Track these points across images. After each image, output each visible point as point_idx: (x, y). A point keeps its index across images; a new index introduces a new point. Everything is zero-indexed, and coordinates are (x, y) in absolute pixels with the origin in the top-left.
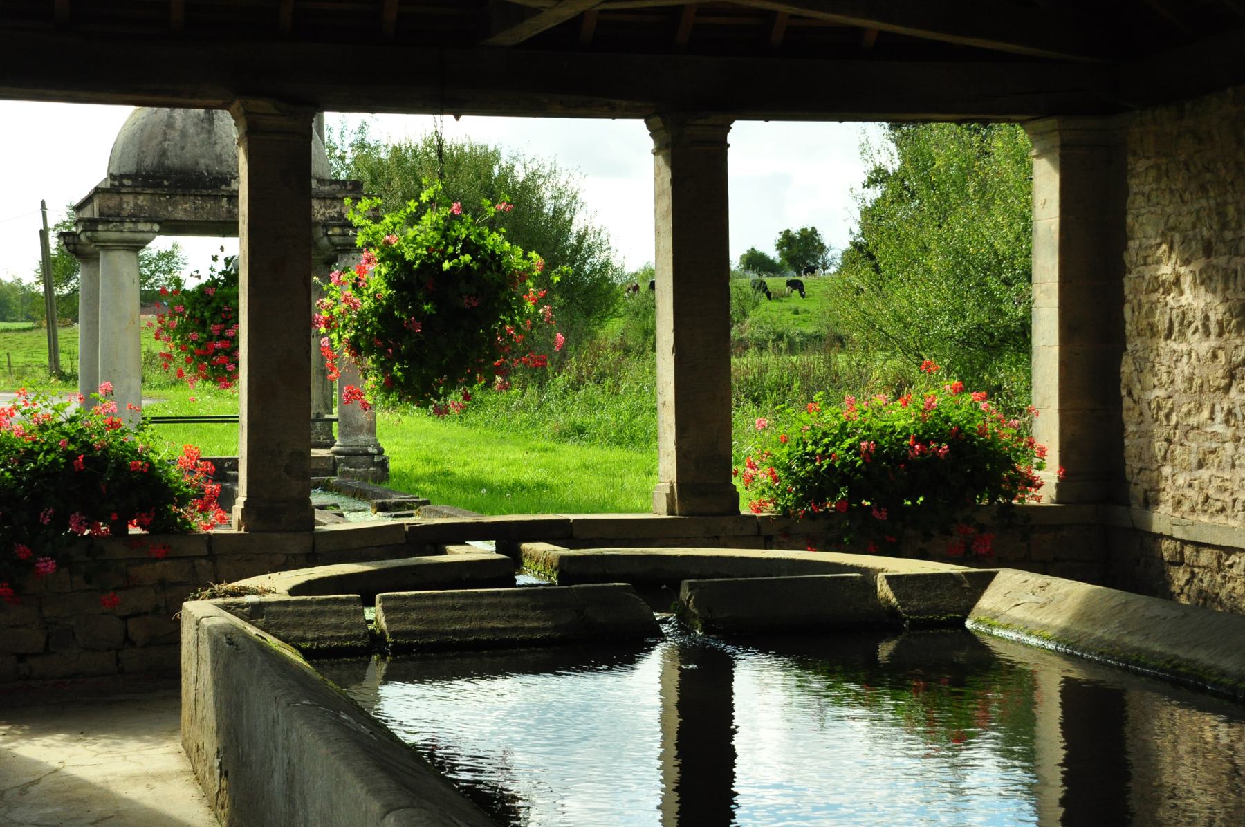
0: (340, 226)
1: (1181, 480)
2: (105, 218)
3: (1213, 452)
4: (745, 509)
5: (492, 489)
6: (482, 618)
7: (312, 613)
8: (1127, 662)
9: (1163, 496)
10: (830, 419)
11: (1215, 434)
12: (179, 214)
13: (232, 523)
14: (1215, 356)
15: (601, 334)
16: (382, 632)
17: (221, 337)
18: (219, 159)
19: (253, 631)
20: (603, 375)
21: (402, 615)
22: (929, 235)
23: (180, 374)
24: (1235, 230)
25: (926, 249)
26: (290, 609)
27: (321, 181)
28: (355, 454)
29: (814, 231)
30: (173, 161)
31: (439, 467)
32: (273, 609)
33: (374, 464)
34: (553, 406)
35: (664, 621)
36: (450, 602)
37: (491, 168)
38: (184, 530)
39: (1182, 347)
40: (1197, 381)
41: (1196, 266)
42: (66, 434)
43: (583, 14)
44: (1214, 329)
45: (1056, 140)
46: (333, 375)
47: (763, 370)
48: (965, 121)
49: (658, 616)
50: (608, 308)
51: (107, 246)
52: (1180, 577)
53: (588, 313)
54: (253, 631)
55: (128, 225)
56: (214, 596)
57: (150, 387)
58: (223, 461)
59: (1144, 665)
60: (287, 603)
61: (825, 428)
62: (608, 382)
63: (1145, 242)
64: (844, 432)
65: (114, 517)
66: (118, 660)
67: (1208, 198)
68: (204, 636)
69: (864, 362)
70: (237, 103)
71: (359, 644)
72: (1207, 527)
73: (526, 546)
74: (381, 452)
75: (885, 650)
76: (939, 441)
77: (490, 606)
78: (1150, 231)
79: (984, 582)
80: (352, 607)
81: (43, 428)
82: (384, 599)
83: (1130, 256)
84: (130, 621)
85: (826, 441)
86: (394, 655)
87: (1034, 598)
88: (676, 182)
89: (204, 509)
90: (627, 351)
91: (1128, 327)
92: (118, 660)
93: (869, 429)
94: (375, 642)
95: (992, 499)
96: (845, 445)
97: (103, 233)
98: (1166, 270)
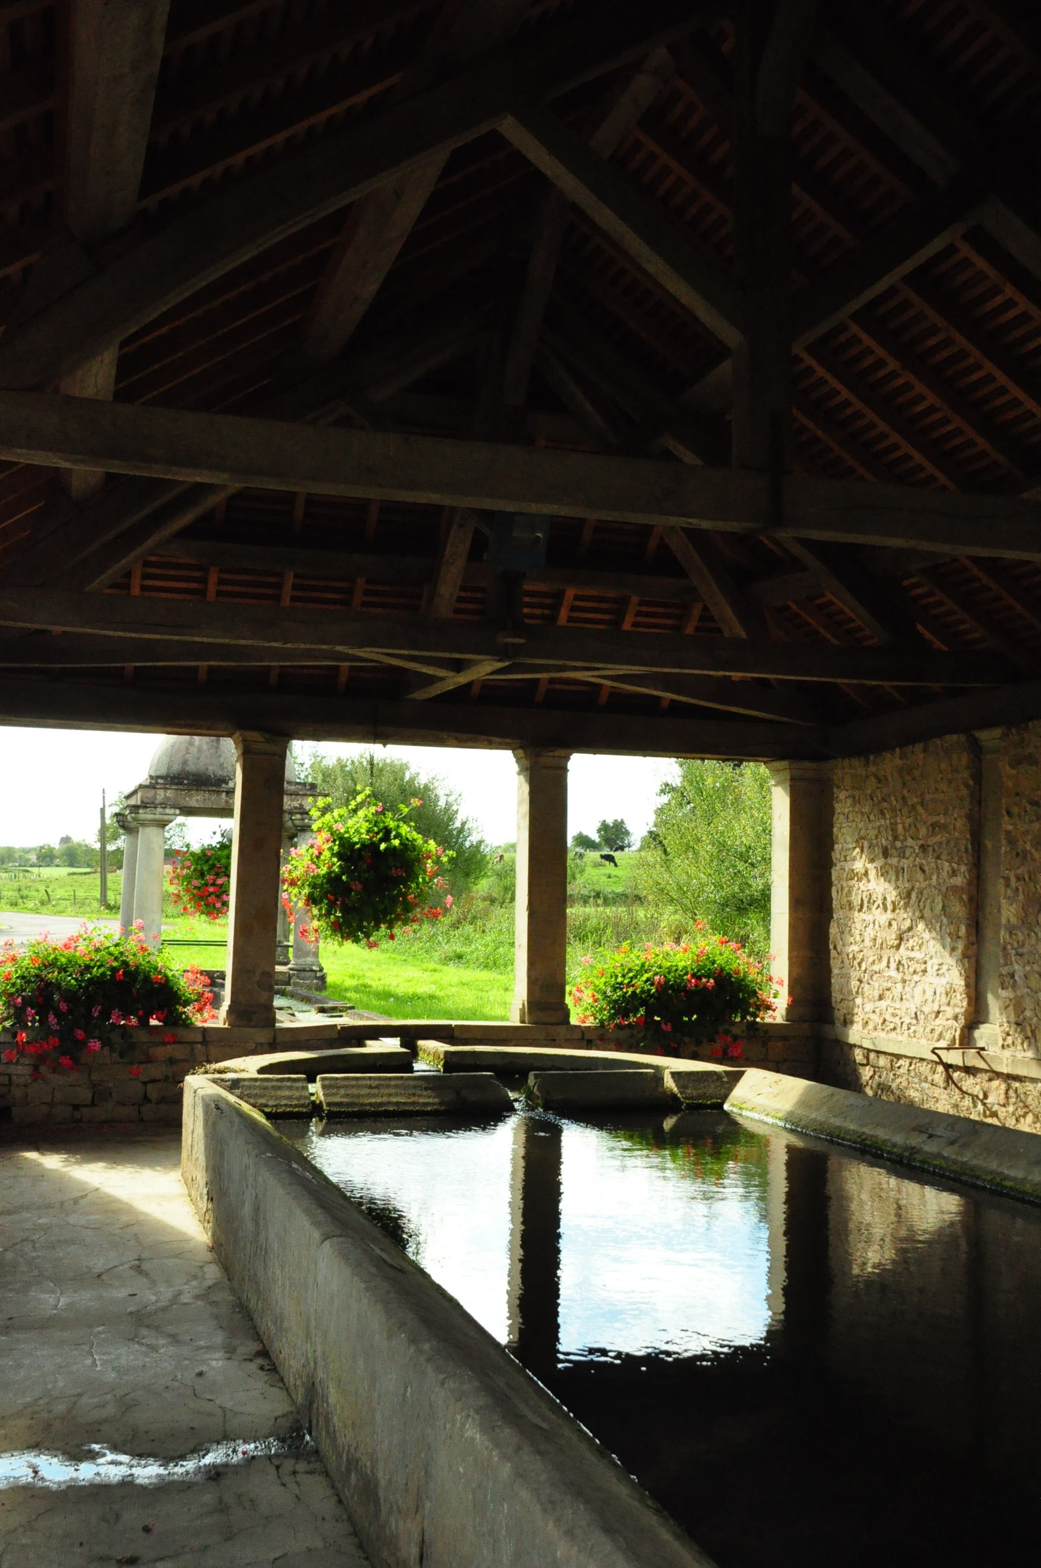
0: (301, 814)
1: (869, 1007)
2: (144, 805)
3: (888, 990)
4: (574, 1021)
5: (397, 998)
6: (390, 1095)
7: (273, 1087)
8: (832, 1136)
9: (856, 1019)
10: (634, 958)
11: (890, 977)
12: (193, 803)
13: (218, 1018)
14: (890, 925)
15: (475, 888)
16: (321, 1102)
17: (213, 884)
18: (222, 766)
19: (232, 1099)
20: (475, 918)
21: (334, 1091)
22: (701, 831)
23: (185, 909)
24: (902, 842)
25: (699, 840)
26: (258, 1084)
27: (289, 783)
28: (304, 970)
29: (622, 822)
30: (192, 768)
31: (361, 982)
32: (246, 1083)
33: (317, 978)
34: (441, 939)
35: (516, 1100)
36: (369, 1082)
37: (404, 774)
38: (185, 1024)
39: (869, 918)
40: (879, 941)
41: (879, 863)
42: (111, 954)
43: (472, 681)
44: (890, 907)
45: (787, 775)
46: (291, 918)
47: (587, 919)
48: (728, 760)
49: (512, 1095)
50: (480, 871)
51: (144, 824)
52: (866, 1073)
53: (467, 875)
54: (232, 1099)
55: (159, 810)
56: (206, 1072)
57: (167, 916)
58: (214, 972)
59: (843, 1139)
60: (256, 1080)
61: (631, 965)
62: (479, 923)
63: (846, 846)
64: (643, 969)
65: (141, 1013)
66: (140, 1112)
67: (885, 819)
68: (199, 1102)
69: (656, 916)
70: (238, 734)
71: (304, 1110)
72: (888, 1042)
73: (421, 1043)
74: (321, 970)
75: (668, 1124)
76: (708, 977)
77: (396, 1086)
78: (849, 839)
79: (737, 1077)
80: (300, 1084)
81: (97, 950)
82: (323, 1079)
83: (836, 855)
84: (149, 1086)
85: (631, 975)
86: (329, 1119)
87: (770, 1090)
88: (533, 794)
89: (200, 1010)
90: (493, 901)
91: (834, 902)
92: (140, 1112)
93: (660, 967)
94: (315, 1109)
95: (743, 1018)
96: (644, 978)
97: (143, 815)
98: (859, 865)
